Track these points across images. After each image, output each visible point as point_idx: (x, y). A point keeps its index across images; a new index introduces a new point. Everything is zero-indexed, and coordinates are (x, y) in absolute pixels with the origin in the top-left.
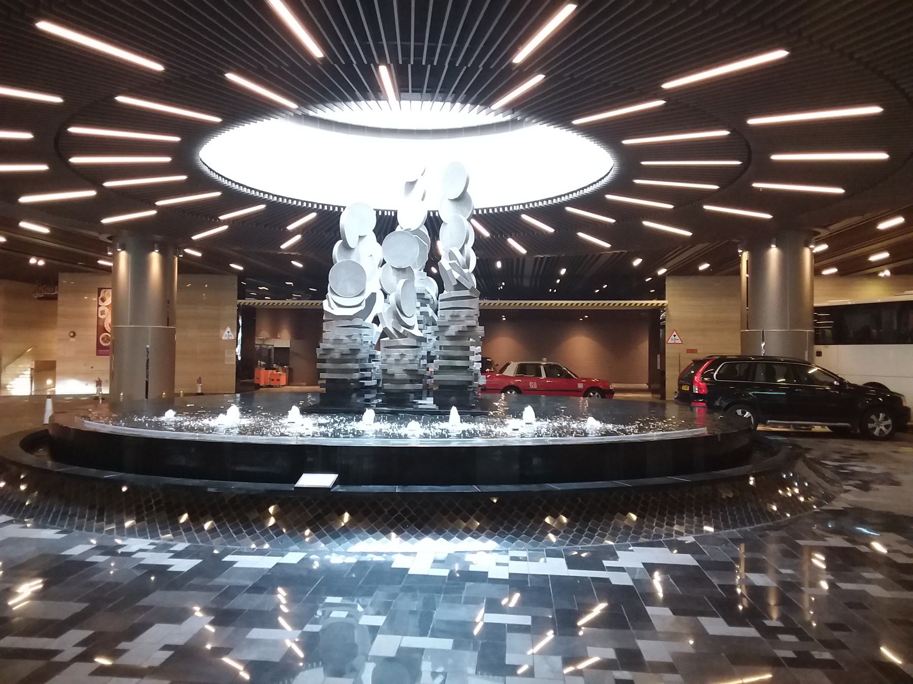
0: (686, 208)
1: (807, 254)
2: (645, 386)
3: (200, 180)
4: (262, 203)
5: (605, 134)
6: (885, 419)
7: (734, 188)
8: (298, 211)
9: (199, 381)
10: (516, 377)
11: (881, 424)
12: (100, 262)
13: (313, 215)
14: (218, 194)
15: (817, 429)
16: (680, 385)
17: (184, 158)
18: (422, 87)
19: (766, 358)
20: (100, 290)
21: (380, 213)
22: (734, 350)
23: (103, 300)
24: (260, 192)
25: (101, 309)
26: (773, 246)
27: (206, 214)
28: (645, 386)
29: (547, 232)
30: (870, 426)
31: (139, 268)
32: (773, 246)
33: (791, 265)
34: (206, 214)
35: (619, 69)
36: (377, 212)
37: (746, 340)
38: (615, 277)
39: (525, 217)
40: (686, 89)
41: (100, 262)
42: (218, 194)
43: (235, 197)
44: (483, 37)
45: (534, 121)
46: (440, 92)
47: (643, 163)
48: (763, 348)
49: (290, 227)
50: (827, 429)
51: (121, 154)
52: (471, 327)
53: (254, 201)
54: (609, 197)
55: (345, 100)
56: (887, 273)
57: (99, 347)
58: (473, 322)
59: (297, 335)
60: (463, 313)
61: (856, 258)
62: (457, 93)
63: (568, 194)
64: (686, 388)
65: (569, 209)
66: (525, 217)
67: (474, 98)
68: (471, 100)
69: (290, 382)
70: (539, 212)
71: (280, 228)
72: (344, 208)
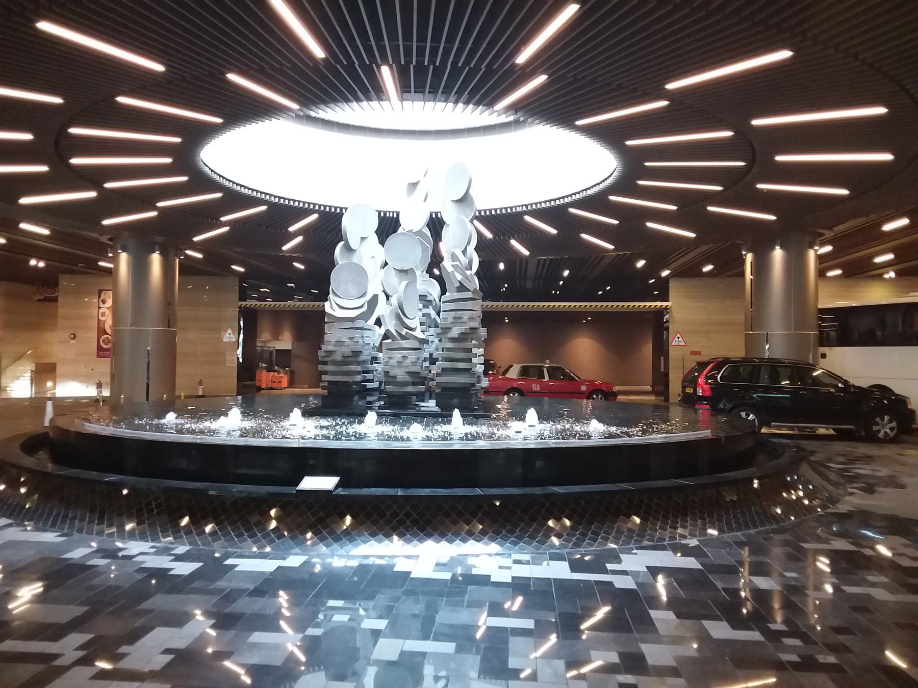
0: (690, 209)
1: (811, 255)
2: (649, 388)
3: (201, 181)
4: (264, 205)
5: (609, 135)
6: (890, 421)
7: (738, 189)
8: (300, 212)
9: (200, 383)
10: (519, 380)
11: (886, 427)
12: (101, 263)
13: (315, 217)
14: (219, 195)
15: (822, 431)
16: (684, 387)
17: (185, 159)
18: (424, 88)
19: (770, 360)
20: (100, 291)
21: (382, 214)
22: (738, 352)
23: (104, 302)
24: (262, 193)
25: (101, 311)
26: (778, 247)
27: (207, 216)
28: (649, 388)
29: (550, 234)
30: (875, 428)
31: (140, 270)
32: (778, 247)
33: (795, 266)
34: (207, 216)
35: (623, 69)
36: (379, 213)
37: (750, 342)
38: (619, 279)
39: (528, 218)
40: (690, 90)
41: (101, 263)
42: (219, 195)
43: (236, 199)
44: (486, 38)
45: (537, 122)
46: (442, 92)
47: (647, 164)
48: (768, 350)
49: (292, 229)
50: (832, 432)
51: (122, 155)
52: (474, 329)
53: (256, 202)
54: (612, 198)
55: (347, 100)
56: (892, 274)
57: (100, 349)
58: (476, 324)
59: (299, 337)
60: (466, 315)
61: (861, 259)
62: (459, 94)
63: (571, 195)
64: (689, 390)
65: (572, 210)
66: (528, 218)
67: (476, 98)
68: (474, 101)
69: (291, 384)
70: (542, 213)
71: (281, 230)
72: (346, 209)
